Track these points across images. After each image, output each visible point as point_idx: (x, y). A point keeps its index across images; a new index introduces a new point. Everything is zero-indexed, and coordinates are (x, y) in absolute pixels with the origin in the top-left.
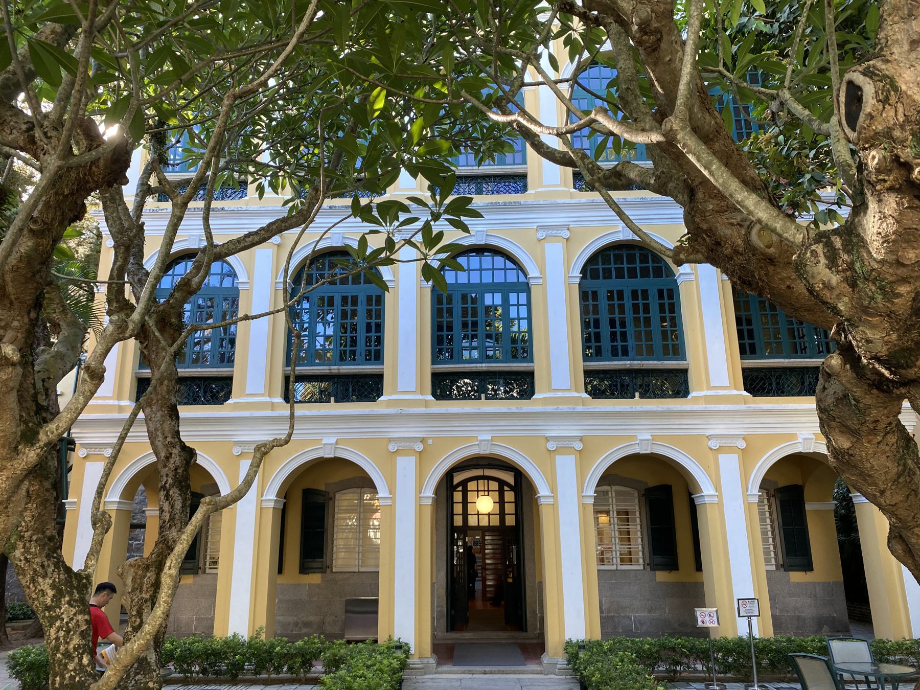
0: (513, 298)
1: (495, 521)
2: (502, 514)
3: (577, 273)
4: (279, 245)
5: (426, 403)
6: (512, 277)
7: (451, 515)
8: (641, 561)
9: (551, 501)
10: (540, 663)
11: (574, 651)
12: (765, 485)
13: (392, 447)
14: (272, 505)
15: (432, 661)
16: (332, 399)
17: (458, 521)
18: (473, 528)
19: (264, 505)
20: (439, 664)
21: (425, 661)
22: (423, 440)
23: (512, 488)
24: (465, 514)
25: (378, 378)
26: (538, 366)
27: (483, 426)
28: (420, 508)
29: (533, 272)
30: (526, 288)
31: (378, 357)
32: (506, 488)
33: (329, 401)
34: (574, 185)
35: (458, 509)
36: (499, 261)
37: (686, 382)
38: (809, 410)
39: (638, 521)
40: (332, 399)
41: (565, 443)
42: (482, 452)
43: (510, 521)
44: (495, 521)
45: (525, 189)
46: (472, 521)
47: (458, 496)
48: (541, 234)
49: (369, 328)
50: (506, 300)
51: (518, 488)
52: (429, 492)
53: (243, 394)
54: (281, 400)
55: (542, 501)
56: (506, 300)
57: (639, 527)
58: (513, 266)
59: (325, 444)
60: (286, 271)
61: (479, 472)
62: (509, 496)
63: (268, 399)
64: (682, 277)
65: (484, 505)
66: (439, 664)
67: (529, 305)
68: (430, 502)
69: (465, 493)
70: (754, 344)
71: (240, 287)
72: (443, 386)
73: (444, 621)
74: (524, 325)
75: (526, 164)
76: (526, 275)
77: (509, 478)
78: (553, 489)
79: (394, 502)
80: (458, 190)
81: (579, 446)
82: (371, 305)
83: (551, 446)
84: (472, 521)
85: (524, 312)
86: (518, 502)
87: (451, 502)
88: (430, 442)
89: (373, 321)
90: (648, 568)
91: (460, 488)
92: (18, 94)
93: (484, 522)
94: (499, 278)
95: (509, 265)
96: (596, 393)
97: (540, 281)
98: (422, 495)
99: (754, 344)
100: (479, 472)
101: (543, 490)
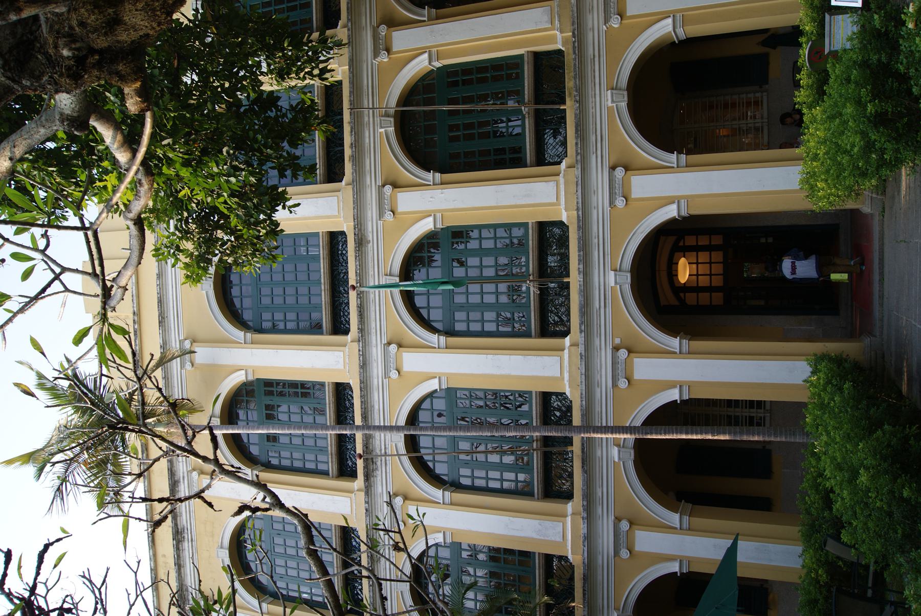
1: (718, 256)
2: (709, 248)
7: (710, 310)
8: (758, 95)
10: (872, 215)
13: (623, 384)
14: (686, 518)
17: (718, 298)
19: (685, 525)
22: (616, 349)
24: (710, 289)
28: (691, 353)
29: (433, 385)
32: (681, 244)
35: (704, 298)
40: (566, 280)
43: (717, 240)
44: (718, 256)
45: (343, 233)
46: (718, 281)
47: (691, 299)
50: (461, 307)
55: (684, 213)
56: (461, 307)
58: (428, 400)
59: (619, 458)
61: (96, 256)
62: (690, 241)
63: (566, 351)
70: (489, 137)
71: (449, 540)
78: (669, 201)
81: (623, 354)
84: (718, 281)
86: (697, 232)
88: (618, 341)
91: (682, 295)
92: (781, 261)
93: (718, 269)
97: (439, 215)
98: (678, 351)
99: (489, 137)
100: (96, 256)
101: (671, 212)
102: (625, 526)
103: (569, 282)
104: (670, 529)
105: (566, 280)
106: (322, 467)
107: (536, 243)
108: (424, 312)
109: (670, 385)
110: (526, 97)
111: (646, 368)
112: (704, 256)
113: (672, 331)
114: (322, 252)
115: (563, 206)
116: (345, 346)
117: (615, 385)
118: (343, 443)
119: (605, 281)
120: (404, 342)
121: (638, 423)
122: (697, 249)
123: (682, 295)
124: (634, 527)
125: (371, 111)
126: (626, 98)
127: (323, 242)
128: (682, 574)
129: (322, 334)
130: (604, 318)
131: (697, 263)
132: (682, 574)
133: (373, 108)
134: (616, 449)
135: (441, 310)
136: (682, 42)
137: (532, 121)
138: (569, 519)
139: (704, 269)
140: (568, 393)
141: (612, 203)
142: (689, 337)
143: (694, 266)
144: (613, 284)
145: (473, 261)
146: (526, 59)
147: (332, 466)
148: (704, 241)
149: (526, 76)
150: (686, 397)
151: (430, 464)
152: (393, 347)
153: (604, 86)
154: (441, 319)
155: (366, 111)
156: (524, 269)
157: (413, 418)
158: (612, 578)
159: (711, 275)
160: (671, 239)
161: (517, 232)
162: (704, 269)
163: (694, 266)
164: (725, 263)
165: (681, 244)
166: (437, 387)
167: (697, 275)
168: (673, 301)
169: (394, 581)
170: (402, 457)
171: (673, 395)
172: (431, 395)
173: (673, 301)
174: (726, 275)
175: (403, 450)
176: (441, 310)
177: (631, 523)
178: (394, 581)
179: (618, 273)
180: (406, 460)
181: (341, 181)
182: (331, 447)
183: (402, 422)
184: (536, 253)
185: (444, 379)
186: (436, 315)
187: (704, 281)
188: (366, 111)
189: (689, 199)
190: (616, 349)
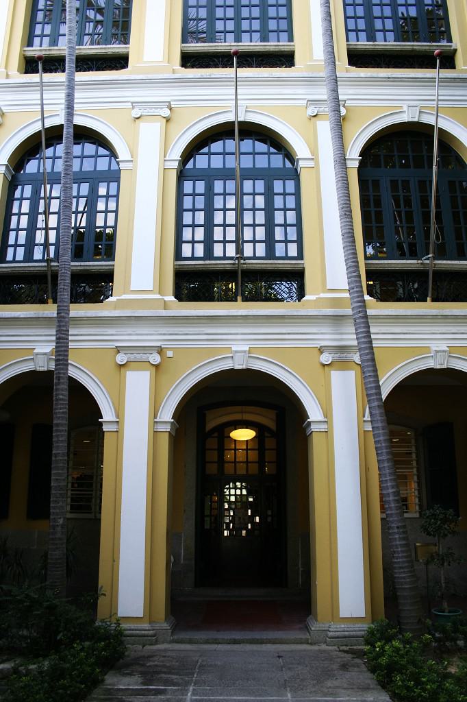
0: (278, 186)
2: (261, 461)
5: (166, 305)
6: (103, 164)
9: (323, 427)
13: (326, 358)
15: (166, 626)
16: (239, 298)
21: (157, 626)
22: (160, 351)
24: (221, 461)
27: (237, 338)
28: (155, 434)
29: (123, 153)
30: (295, 176)
32: (266, 434)
33: (236, 301)
35: (212, 456)
38: (456, 317)
39: (414, 463)
40: (239, 298)
47: (212, 443)
53: (127, 290)
54: (173, 299)
55: (313, 427)
57: (415, 471)
58: (107, 153)
60: (342, 160)
62: (270, 443)
63: (158, 296)
66: (176, 628)
68: (168, 428)
75: (292, 41)
79: (317, 164)
83: (121, 358)
88: (170, 354)
91: (216, 435)
94: (262, 162)
96: (182, 293)
98: (158, 420)
99: (457, 239)
101: (314, 413)
102: (155, 359)
104: (155, 412)
106: (37, 41)
107: (443, 268)
109: (119, 412)
110: (440, 262)
111: (138, 384)
112: (253, 456)
114: (272, 45)
115: (322, 295)
116: (168, 62)
117: (118, 350)
118: (53, 64)
119: (237, 338)
120: (171, 125)
121: (72, 372)
124: (154, 368)
125: (435, 98)
127: (282, 45)
128: (101, 424)
129: (22, 46)
130: (195, 337)
131: (247, 450)
132: (101, 424)
133: (438, 100)
134: (247, 348)
137: (228, 267)
138: (158, 296)
140: (111, 299)
142: (174, 434)
143: (245, 447)
147: (35, 51)
148: (270, 456)
150: (105, 428)
151: (205, 150)
152: (167, 113)
155: (435, 92)
157: (84, 135)
163: (245, 447)
165: (266, 434)
166: (121, 158)
167: (235, 450)
168: (210, 425)
169: (42, 108)
170: (40, 123)
171: (107, 414)
172: (113, 154)
173: (210, 425)
175: (49, 123)
177: (157, 367)
178: (42, 108)
179: (247, 354)
180: (37, 127)
181: (349, 64)
182: (55, 52)
183: (78, 121)
184: (269, 267)
185: (129, 165)
186: (201, 161)
187: (229, 456)
188: (435, 92)
189: (328, 434)
190: (160, 351)
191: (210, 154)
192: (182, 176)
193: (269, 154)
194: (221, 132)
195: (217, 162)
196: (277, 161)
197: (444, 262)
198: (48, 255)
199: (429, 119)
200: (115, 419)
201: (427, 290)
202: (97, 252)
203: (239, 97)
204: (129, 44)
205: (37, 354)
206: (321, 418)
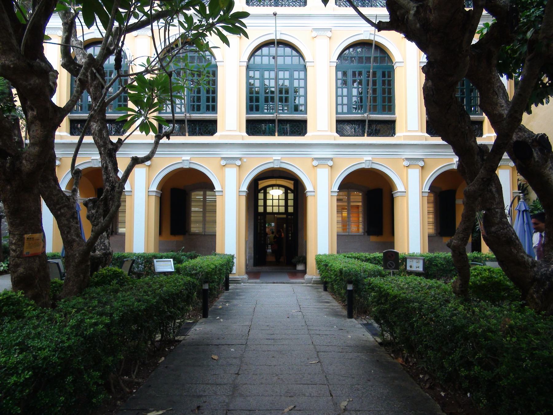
0: (296, 74)
1: (282, 210)
2: (286, 206)
3: (336, 189)
4: (149, 166)
5: (243, 138)
7: (256, 206)
11: (323, 265)
12: (433, 188)
17: (261, 209)
18: (270, 213)
20: (249, 279)
23: (292, 191)
24: (265, 206)
25: (214, 122)
26: (310, 117)
27: (276, 151)
30: (305, 69)
31: (214, 109)
32: (289, 191)
34: (336, 2)
35: (261, 203)
36: (288, 50)
37: (394, 129)
40: (276, 134)
41: (323, 160)
42: (275, 167)
43: (291, 210)
44: (282, 210)
46: (269, 210)
47: (261, 196)
48: (315, 163)
49: (208, 100)
51: (297, 190)
52: (244, 188)
55: (308, 194)
56: (291, 76)
58: (297, 54)
62: (291, 196)
64: (397, 64)
65: (276, 195)
66: (249, 279)
67: (305, 79)
68: (245, 194)
69: (265, 194)
72: (253, 127)
73: (252, 261)
74: (302, 101)
76: (304, 60)
77: (290, 184)
80: (264, 3)
82: (209, 102)
84: (269, 210)
85: (302, 83)
86: (296, 200)
87: (256, 200)
88: (245, 160)
89: (211, 95)
90: (366, 234)
91: (262, 191)
93: (276, 210)
94: (288, 61)
95: (294, 53)
98: (240, 190)
101: (309, 187)
103: (185, 135)
105: (276, 134)
107: (374, 119)
108: (259, 53)
112: (282, 203)
113: (249, 188)
122: (286, 199)
123: (262, 191)
126: (367, 167)
135: (290, 63)
136: (392, 195)
137: (271, 118)
139: (276, 203)
141: (223, 158)
144: (274, 158)
145: (296, 84)
146: (393, 116)
148: (291, 203)
149: (383, 116)
153: (375, 157)
154: (263, 63)
156: (266, 111)
158: (163, 156)
159: (273, 206)
160: (292, 187)
161: (302, 108)
162: (276, 203)
164: (279, 213)
165: (289, 191)
168: (260, 187)
173: (260, 187)
174: (273, 213)
176: (290, 63)
177: (422, 167)
191: (262, 56)
192: (248, 68)
193: (292, 56)
194: (269, 44)
195: (265, 60)
196: (296, 60)
197: (375, 116)
198: (345, 206)
199: (372, 38)
200: (221, 190)
201: (184, 128)
202: (208, 109)
203: (277, 25)
204: (217, 113)
205: (184, 160)
206: (312, 190)
